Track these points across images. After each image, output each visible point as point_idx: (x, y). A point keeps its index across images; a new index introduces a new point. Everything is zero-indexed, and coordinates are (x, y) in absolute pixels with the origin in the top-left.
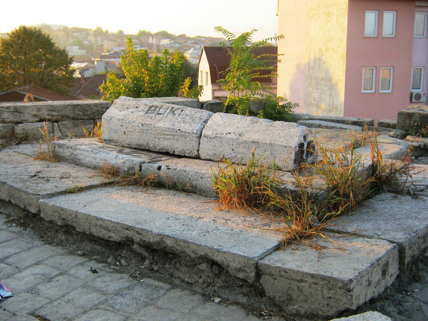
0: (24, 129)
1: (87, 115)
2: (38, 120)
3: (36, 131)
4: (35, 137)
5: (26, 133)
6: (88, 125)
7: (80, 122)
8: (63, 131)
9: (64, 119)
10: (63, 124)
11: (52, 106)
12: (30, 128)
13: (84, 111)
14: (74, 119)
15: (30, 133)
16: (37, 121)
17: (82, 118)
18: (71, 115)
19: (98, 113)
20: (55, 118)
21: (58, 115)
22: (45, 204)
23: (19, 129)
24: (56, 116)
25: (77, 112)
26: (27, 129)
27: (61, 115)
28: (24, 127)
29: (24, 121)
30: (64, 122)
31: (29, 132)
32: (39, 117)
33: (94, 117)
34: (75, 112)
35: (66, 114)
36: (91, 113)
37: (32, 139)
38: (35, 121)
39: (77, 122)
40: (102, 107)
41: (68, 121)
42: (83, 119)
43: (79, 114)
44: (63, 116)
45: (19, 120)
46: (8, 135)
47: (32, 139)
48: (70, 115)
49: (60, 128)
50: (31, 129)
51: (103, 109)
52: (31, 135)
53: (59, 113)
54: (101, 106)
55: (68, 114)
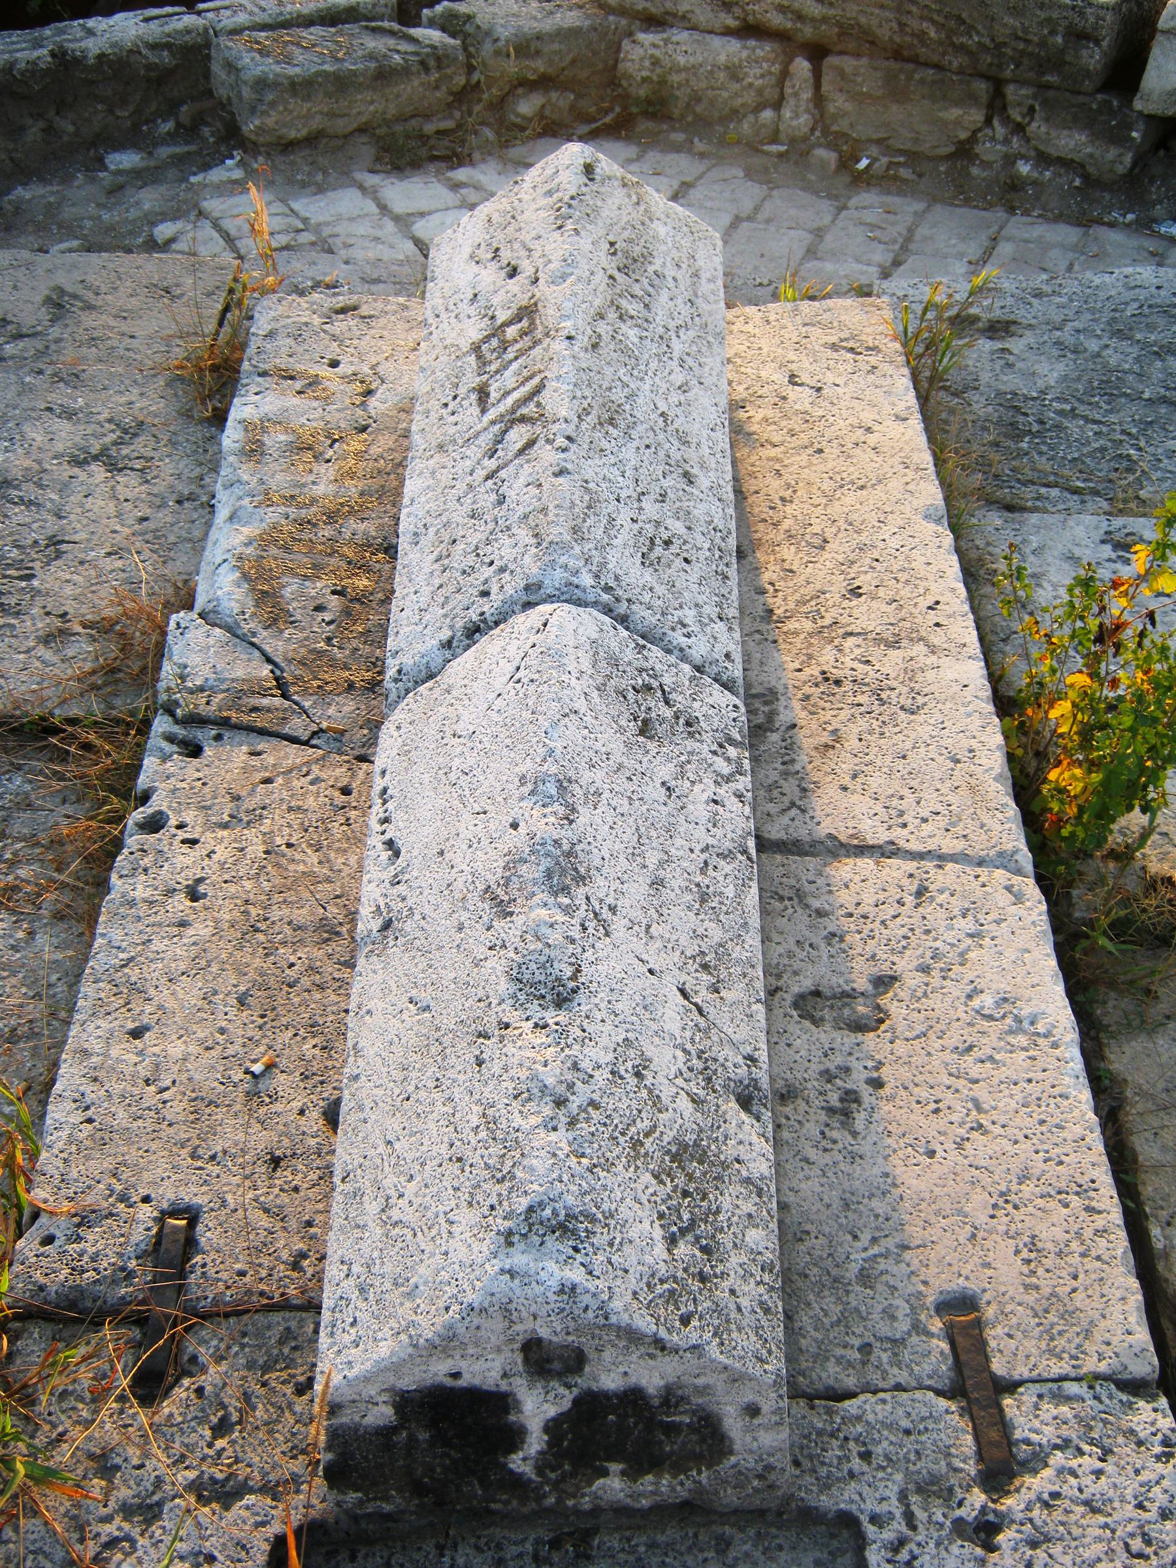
0: (656, 62)
1: (962, 48)
2: (732, 23)
3: (703, 85)
4: (698, 109)
5: (663, 82)
6: (957, 103)
7: (922, 81)
8: (831, 108)
9: (852, 46)
10: (842, 74)
11: (451, 10)
12: (682, 60)
13: (952, 23)
14: (897, 54)
15: (680, 85)
16: (728, 32)
17: (935, 58)
18: (885, 33)
19: (1022, 53)
20: (808, 32)
21: (824, 20)
22: (187, 143)
23: (642, 50)
24: (813, 20)
25: (914, 24)
26: (666, 62)
27: (839, 24)
28: (657, 52)
29: (675, 15)
30: (848, 63)
31: (675, 78)
32: (737, 11)
33: (1000, 66)
34: (904, 19)
35: (863, 20)
36: (987, 41)
37: (682, 117)
38: (718, 26)
39: (910, 78)
40: (1049, 20)
41: (864, 61)
42: (938, 67)
43: (922, 36)
44: (845, 30)
45: (653, 10)
46: (583, 75)
47: (682, 117)
48: (878, 32)
49: (825, 88)
50: (686, 69)
51: (1053, 32)
52: (682, 94)
53: (832, 12)
54: (1043, 15)
55: (874, 22)
